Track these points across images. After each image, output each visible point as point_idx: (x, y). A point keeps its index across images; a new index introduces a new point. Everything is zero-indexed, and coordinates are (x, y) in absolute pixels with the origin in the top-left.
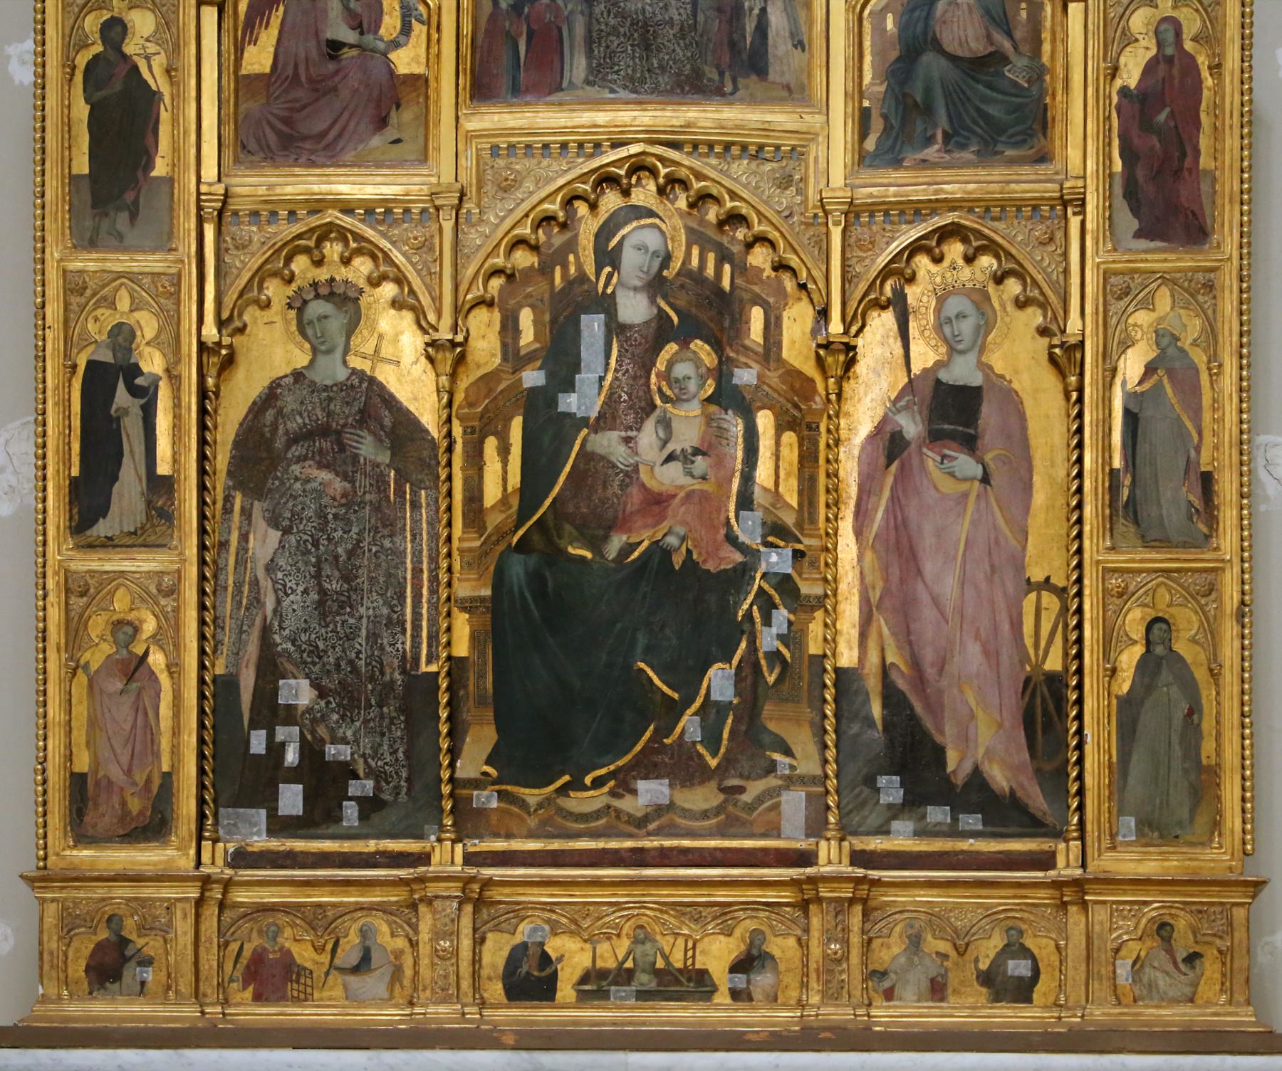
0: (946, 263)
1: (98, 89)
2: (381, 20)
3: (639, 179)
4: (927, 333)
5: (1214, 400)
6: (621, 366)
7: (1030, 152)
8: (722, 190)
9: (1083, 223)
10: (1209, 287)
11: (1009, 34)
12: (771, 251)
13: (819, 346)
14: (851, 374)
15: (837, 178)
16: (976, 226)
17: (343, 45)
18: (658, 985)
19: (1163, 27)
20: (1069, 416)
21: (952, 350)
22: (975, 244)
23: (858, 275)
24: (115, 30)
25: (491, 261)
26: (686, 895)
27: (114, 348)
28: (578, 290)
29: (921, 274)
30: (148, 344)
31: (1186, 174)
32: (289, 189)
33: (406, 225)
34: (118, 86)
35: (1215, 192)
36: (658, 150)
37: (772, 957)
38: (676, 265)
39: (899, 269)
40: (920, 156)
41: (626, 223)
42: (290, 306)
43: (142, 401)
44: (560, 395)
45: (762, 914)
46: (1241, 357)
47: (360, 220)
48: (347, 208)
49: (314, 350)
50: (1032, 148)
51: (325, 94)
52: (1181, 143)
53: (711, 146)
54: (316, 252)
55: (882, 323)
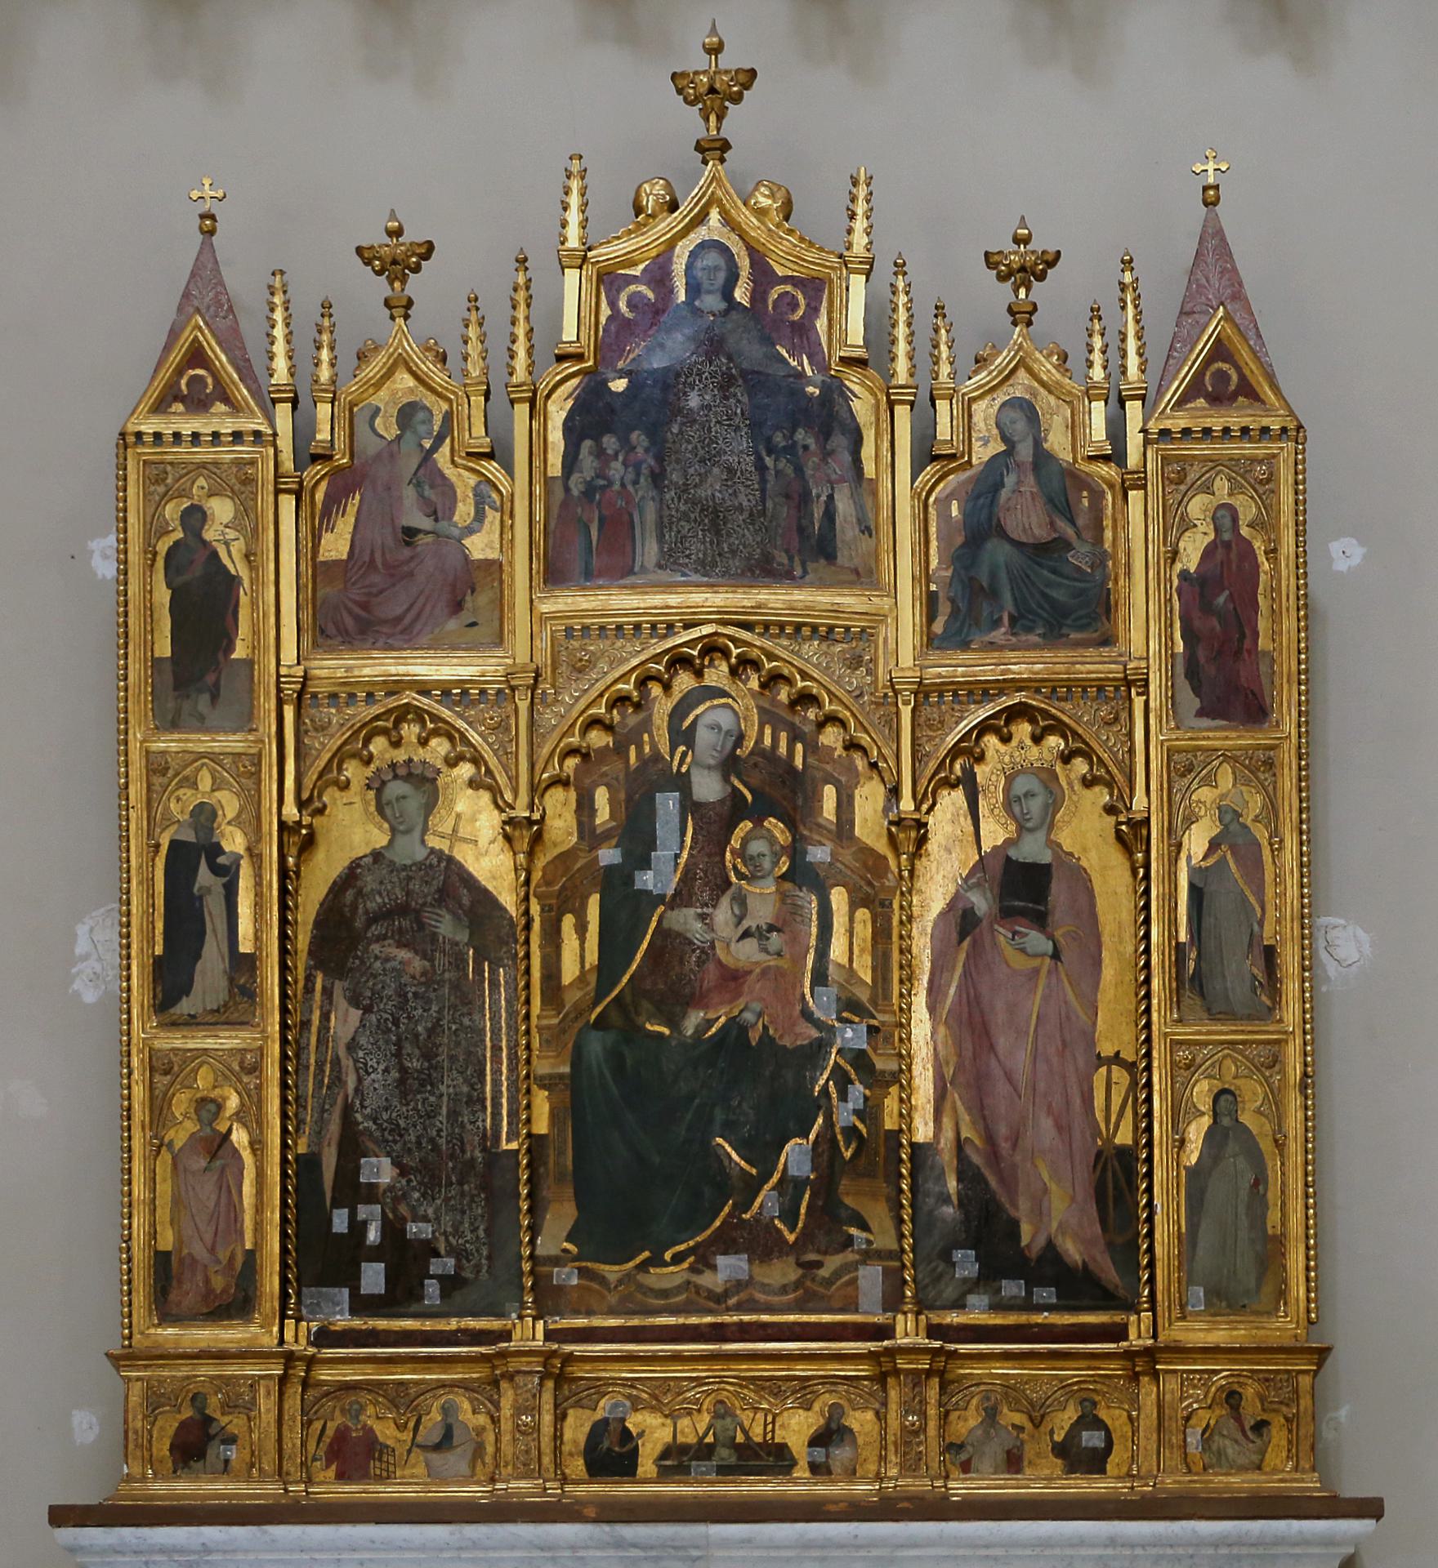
0: (1014, 743)
2: (455, 507)
3: (712, 660)
4: (996, 811)
7: (1095, 635)
9: (1147, 703)
10: (1269, 764)
13: (891, 823)
15: (907, 658)
18: (739, 1459)
21: (1021, 829)
23: (928, 755)
24: (195, 517)
26: (765, 1370)
29: (989, 754)
30: (229, 823)
31: (1246, 655)
34: (198, 570)
36: (730, 630)
37: (851, 1431)
38: (750, 744)
39: (969, 750)
42: (369, 787)
45: (841, 1388)
46: (1301, 833)
47: (437, 701)
48: (424, 688)
49: (393, 830)
52: (1241, 626)
53: (782, 626)
54: (394, 733)
55: (952, 801)
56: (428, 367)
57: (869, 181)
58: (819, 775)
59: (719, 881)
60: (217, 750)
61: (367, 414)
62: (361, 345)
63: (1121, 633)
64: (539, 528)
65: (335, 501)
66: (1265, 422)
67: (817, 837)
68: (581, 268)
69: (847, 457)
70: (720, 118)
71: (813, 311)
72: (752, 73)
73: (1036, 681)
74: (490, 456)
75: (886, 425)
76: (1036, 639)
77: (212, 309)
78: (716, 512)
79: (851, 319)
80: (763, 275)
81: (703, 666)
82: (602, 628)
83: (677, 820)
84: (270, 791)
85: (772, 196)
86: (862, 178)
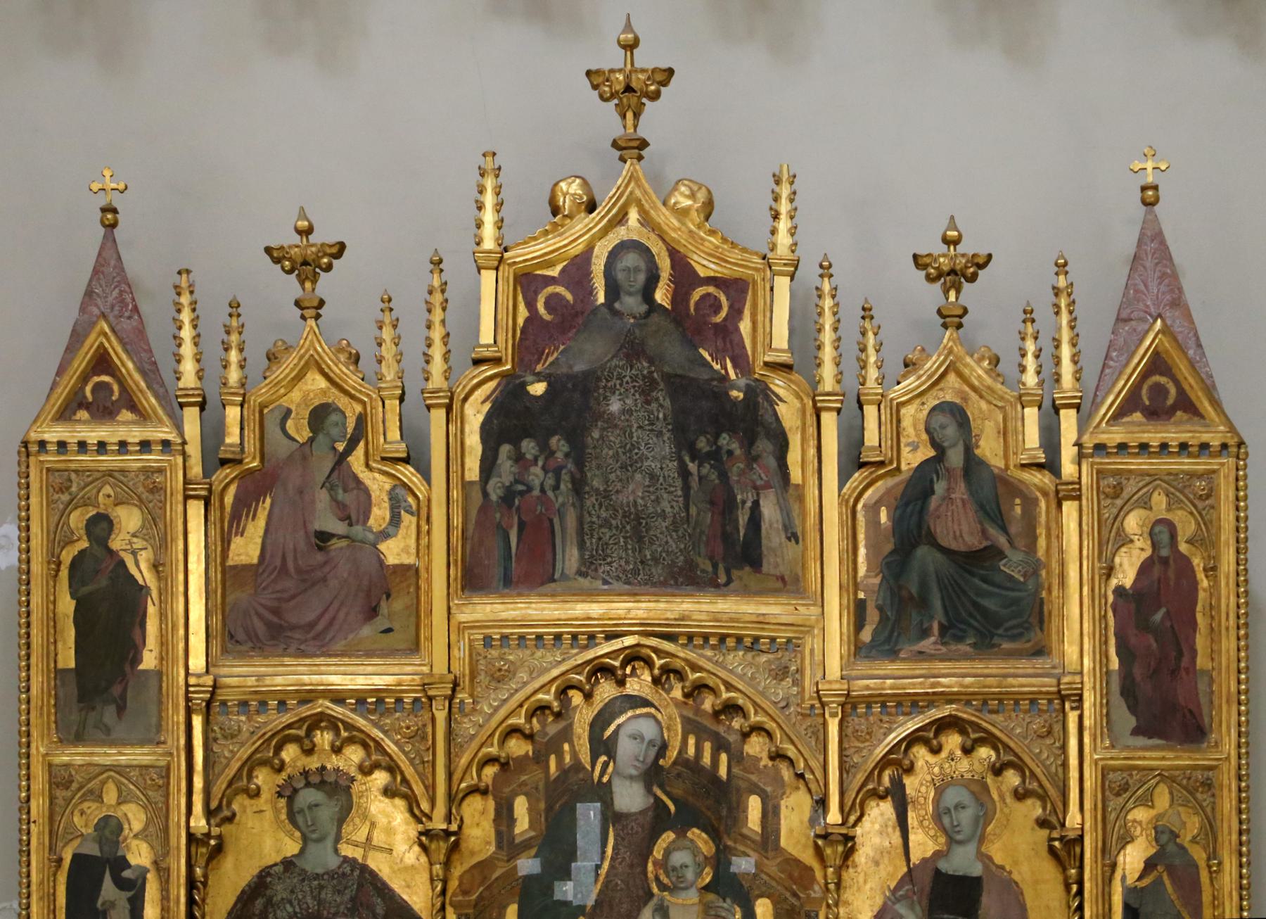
0: (944, 754)
1: (84, 584)
2: (370, 512)
3: (634, 669)
4: (926, 823)
5: (1214, 898)
6: (617, 854)
7: (1028, 645)
8: (718, 681)
9: (1081, 717)
10: (1208, 785)
11: (1004, 529)
12: (767, 740)
13: (817, 836)
14: (850, 863)
15: (834, 667)
16: (973, 719)
17: (332, 536)
19: (1157, 529)
20: (1069, 907)
21: (951, 841)
22: (973, 736)
23: (855, 766)
24: (101, 526)
25: (485, 750)
27: (100, 841)
28: (573, 778)
29: (920, 764)
30: (136, 836)
31: (1183, 673)
32: (279, 680)
33: (398, 714)
34: (103, 582)
35: (1212, 692)
36: (653, 642)
38: (673, 754)
39: (898, 761)
40: (917, 648)
41: (622, 712)
42: (280, 795)
43: (130, 894)
44: (557, 883)
46: (1241, 854)
47: (353, 711)
48: (338, 697)
49: (305, 838)
50: (1029, 641)
51: (313, 584)
52: (1178, 644)
53: (706, 637)
54: (306, 742)
55: (880, 813)
56: (342, 370)
57: (792, 179)
58: (743, 785)
59: (641, 893)
60: (123, 763)
61: (278, 415)
62: (270, 346)
63: (1054, 645)
64: (456, 535)
65: (244, 505)
66: (1205, 437)
67: (741, 848)
68: (497, 269)
69: (772, 462)
70: (637, 116)
71: (736, 313)
72: (670, 72)
73: (966, 694)
74: (406, 461)
75: (812, 430)
76: (968, 649)
77: (117, 308)
78: (638, 518)
79: (773, 326)
80: (684, 275)
81: (625, 676)
82: (522, 637)
83: (598, 831)
84: (179, 805)
85: (692, 196)
86: (785, 177)
